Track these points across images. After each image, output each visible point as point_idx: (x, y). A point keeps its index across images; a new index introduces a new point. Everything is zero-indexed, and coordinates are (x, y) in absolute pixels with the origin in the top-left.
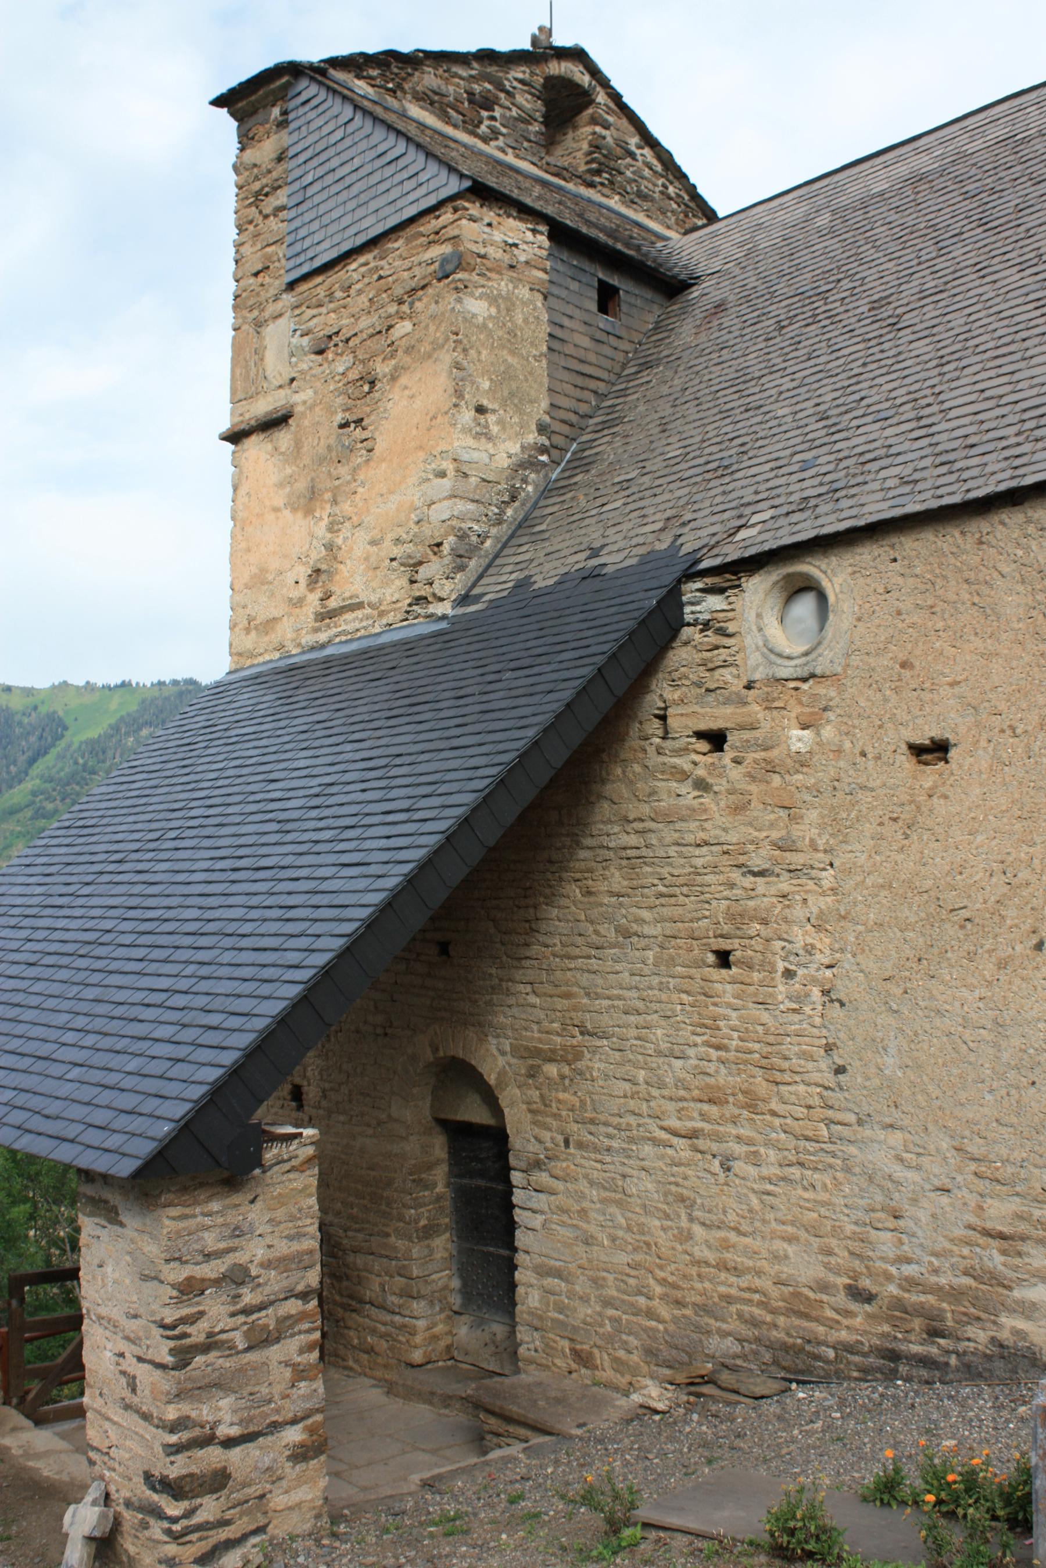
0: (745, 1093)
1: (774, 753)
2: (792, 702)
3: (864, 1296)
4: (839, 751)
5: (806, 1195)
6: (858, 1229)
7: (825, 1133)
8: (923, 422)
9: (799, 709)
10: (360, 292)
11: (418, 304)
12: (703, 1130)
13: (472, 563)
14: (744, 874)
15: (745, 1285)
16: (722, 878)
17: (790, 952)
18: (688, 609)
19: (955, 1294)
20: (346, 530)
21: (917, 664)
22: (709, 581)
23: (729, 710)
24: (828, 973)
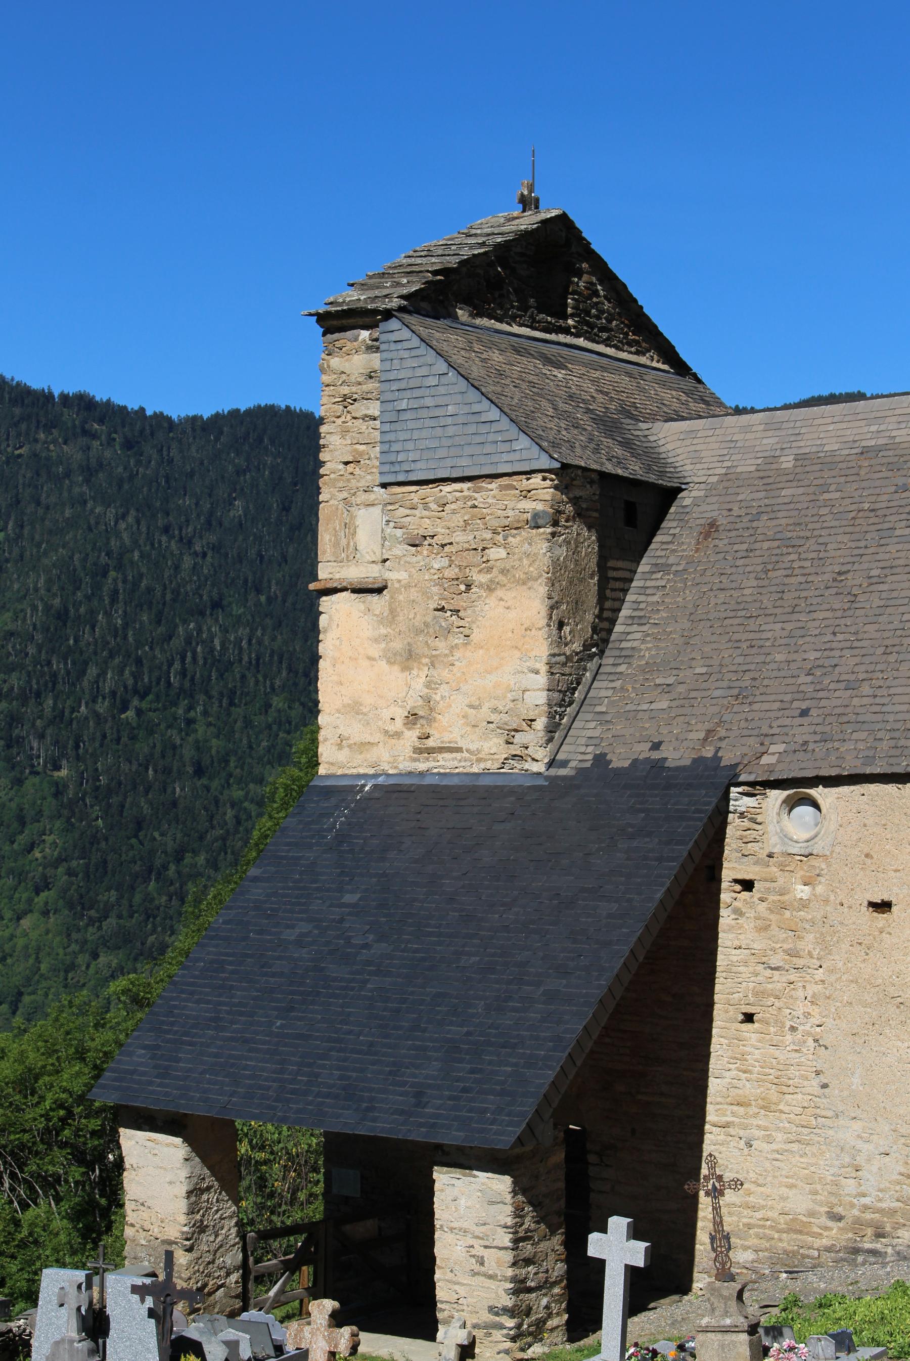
0: (763, 1099)
1: (786, 898)
3: (839, 1218)
4: (826, 901)
5: (802, 1160)
6: (833, 1178)
7: (814, 1123)
8: (878, 700)
10: (454, 512)
11: (510, 539)
12: (733, 1122)
13: (557, 735)
14: (765, 968)
15: (761, 1216)
16: (751, 969)
17: (794, 1017)
18: (732, 802)
19: (893, 1212)
20: (444, 690)
21: (875, 857)
22: (746, 788)
23: (757, 868)
24: (818, 1029)
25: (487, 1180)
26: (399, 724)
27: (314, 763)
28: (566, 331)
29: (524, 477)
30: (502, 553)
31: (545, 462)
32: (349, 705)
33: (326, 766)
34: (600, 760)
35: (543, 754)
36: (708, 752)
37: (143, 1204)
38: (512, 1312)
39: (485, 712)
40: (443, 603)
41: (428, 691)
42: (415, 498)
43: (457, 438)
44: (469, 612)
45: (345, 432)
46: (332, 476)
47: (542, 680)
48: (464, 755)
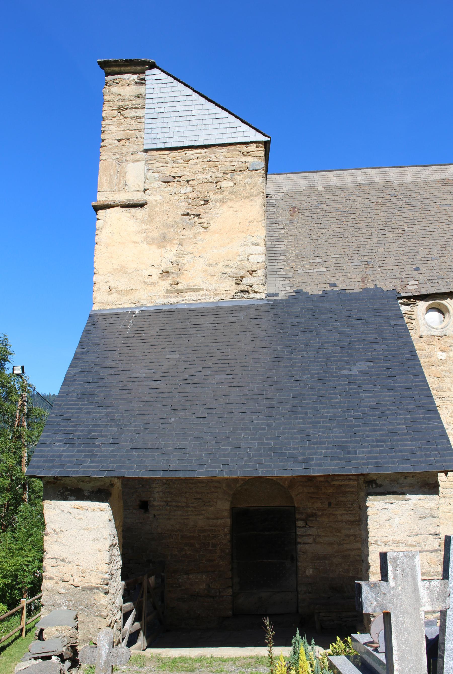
1: (432, 359)
2: (437, 343)
5: (447, 507)
9: (440, 346)
22: (406, 301)
25: (418, 501)
26: (155, 278)
29: (245, 145)
30: (231, 184)
32: (117, 269)
33: (99, 305)
37: (63, 561)
39: (220, 268)
40: (188, 211)
41: (177, 259)
42: (168, 158)
43: (199, 126)
44: (207, 215)
46: (109, 146)
48: (204, 293)
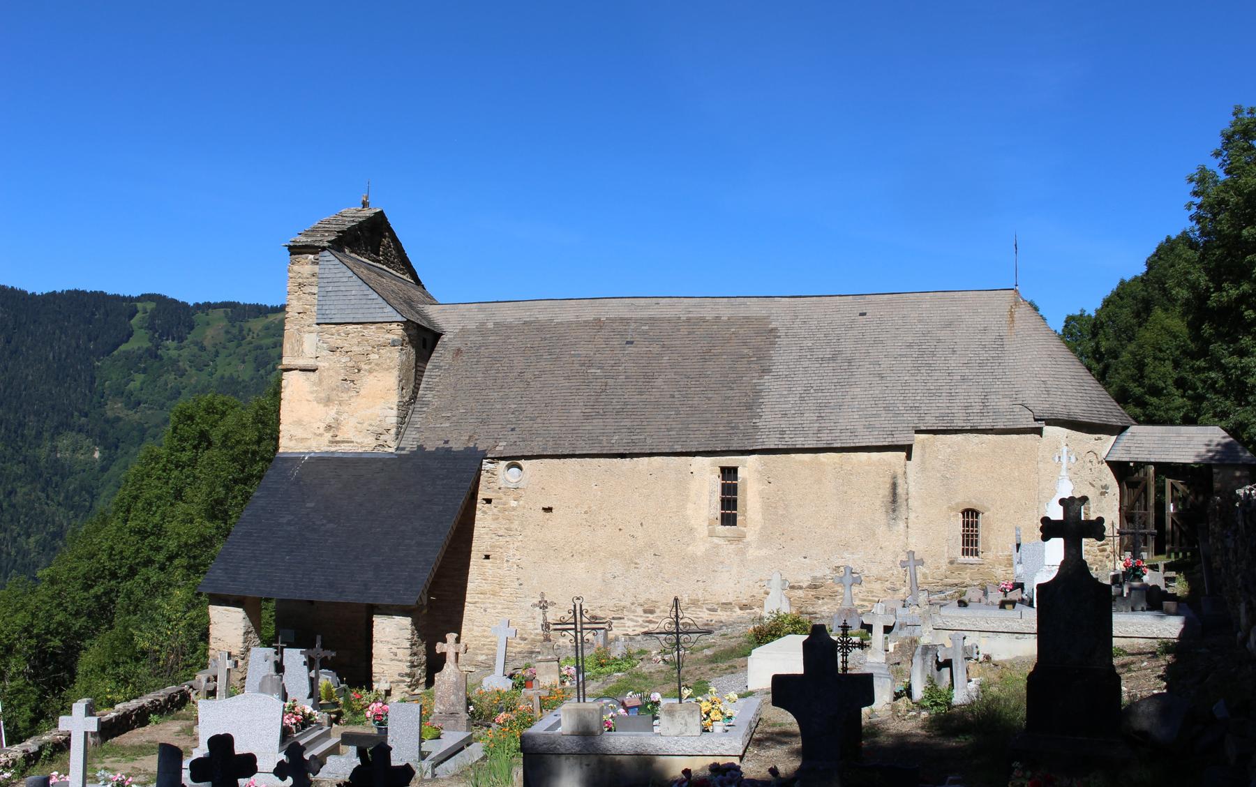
20: (345, 415)
26: (321, 430)
27: (277, 448)
28: (379, 262)
31: (399, 318)
34: (420, 447)
35: (394, 445)
36: (471, 445)
38: (408, 675)
45: (299, 299)
47: (395, 412)
